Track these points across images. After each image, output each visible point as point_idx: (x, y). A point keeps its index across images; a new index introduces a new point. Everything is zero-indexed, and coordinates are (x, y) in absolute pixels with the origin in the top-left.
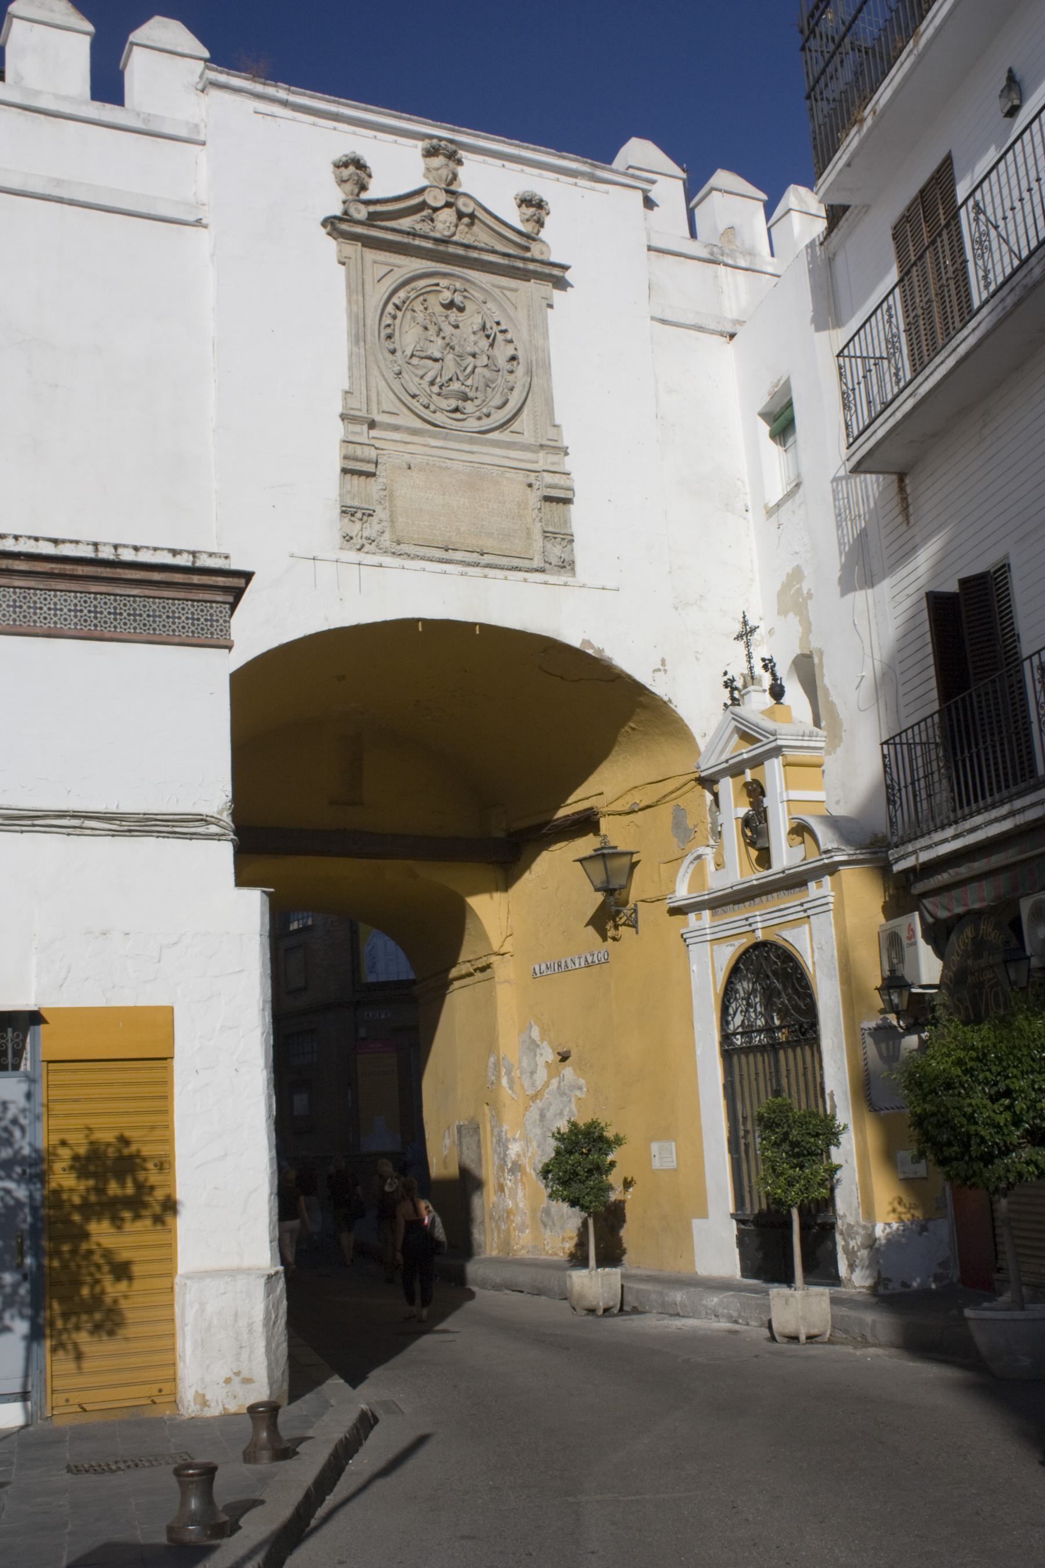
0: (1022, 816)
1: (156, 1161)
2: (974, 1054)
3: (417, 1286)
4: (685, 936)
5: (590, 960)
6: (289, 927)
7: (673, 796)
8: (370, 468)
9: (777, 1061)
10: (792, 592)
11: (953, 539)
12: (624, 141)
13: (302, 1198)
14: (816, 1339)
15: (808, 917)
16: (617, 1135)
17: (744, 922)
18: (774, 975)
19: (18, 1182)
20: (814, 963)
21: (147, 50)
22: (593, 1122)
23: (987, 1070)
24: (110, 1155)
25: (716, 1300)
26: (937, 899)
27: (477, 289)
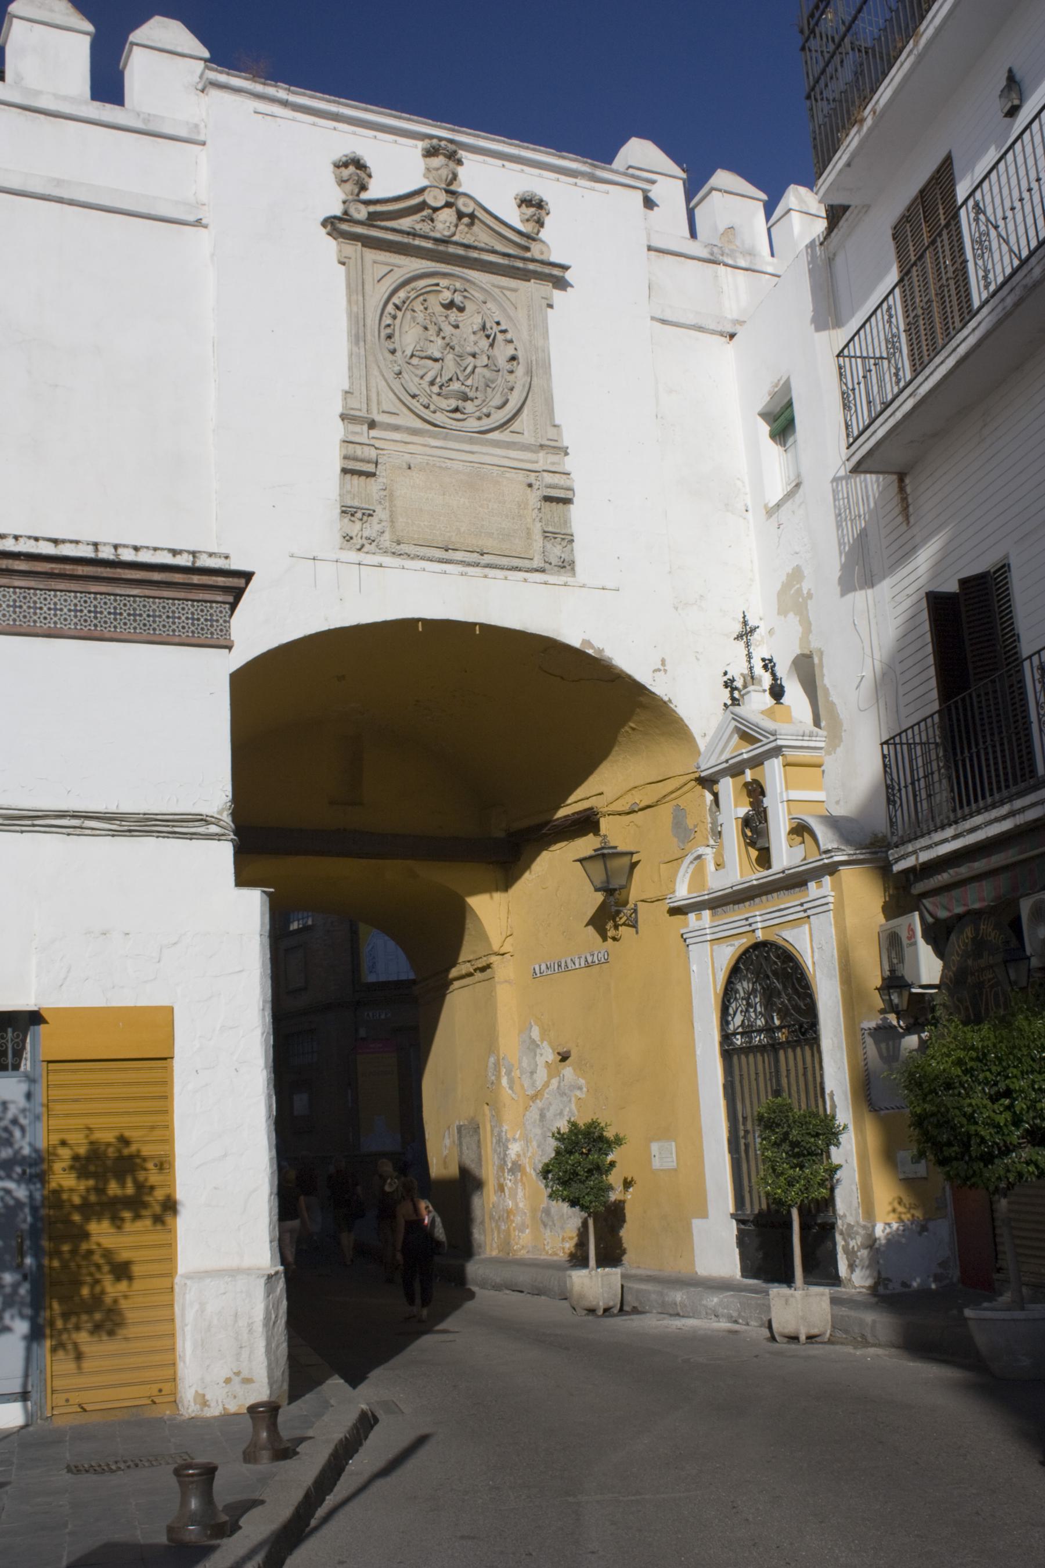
0: (1022, 816)
1: (156, 1161)
2: (974, 1054)
3: (417, 1286)
4: (685, 936)
5: (590, 960)
6: (289, 927)
7: (673, 796)
8: (370, 468)
9: (777, 1061)
10: (792, 592)
11: (953, 539)
12: (624, 141)
13: (302, 1198)
14: (816, 1339)
15: (808, 917)
16: (617, 1135)
17: (744, 922)
18: (774, 975)
19: (18, 1182)
20: (814, 963)
21: (147, 50)
22: (593, 1122)
23: (987, 1070)
24: (110, 1155)
25: (716, 1300)
26: (937, 899)
27: (477, 289)
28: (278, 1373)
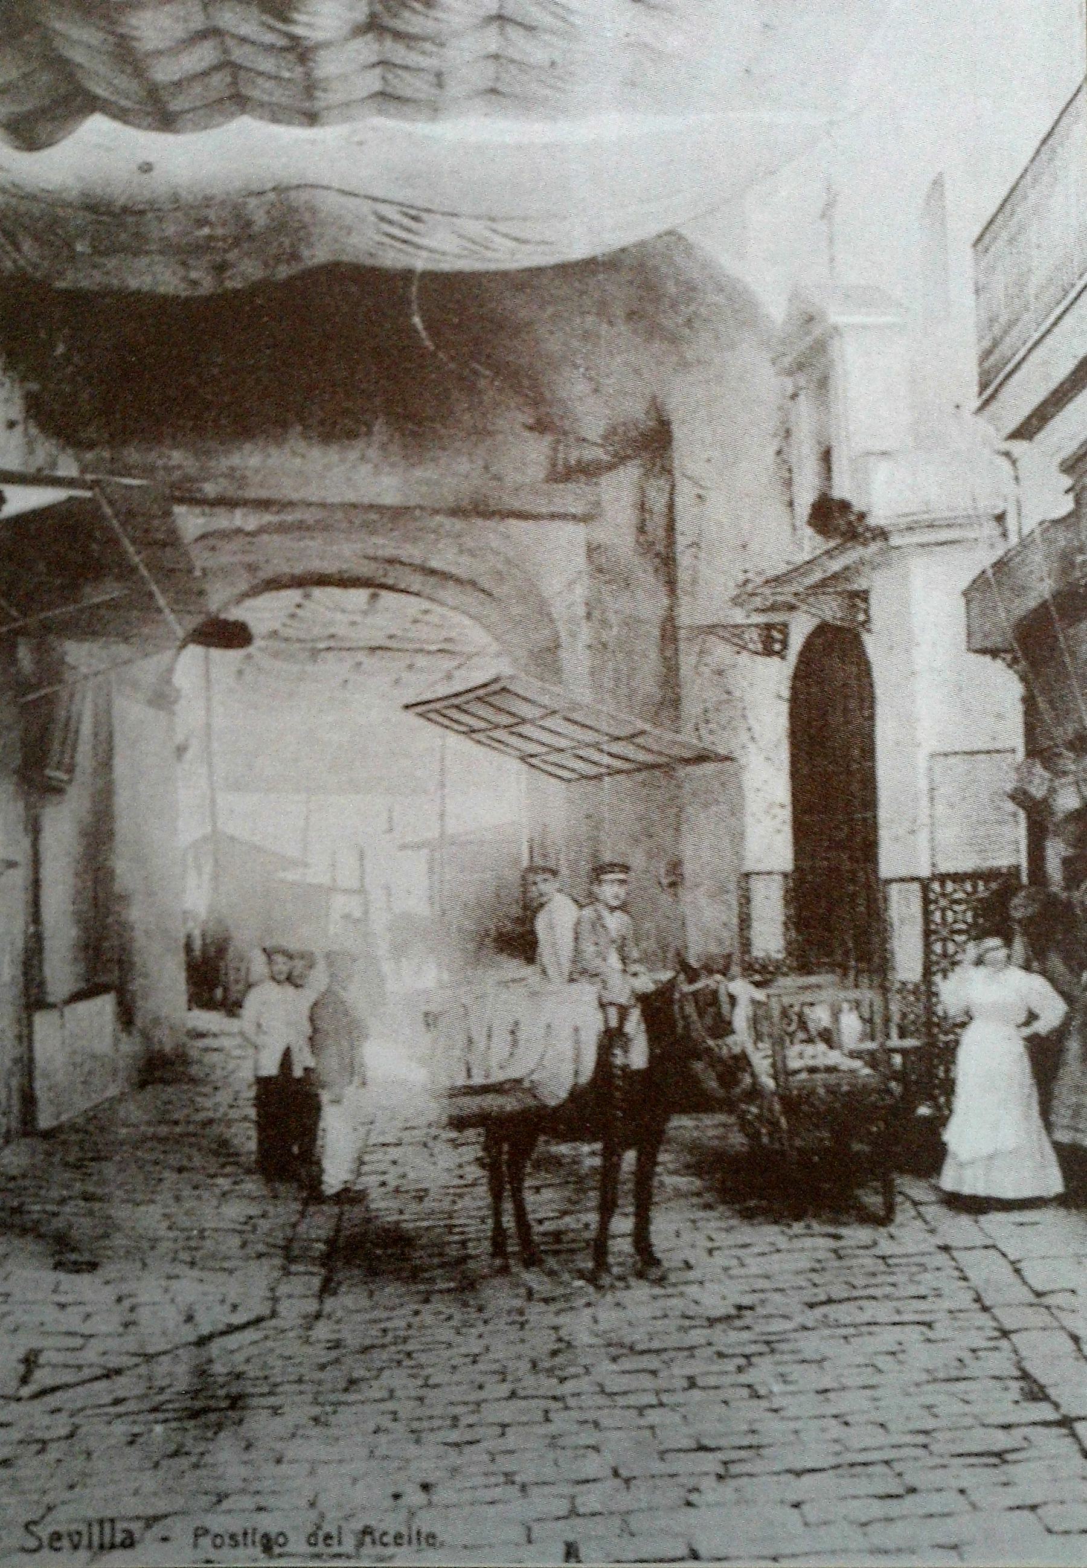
13: (48, 772)
28: (392, 111)
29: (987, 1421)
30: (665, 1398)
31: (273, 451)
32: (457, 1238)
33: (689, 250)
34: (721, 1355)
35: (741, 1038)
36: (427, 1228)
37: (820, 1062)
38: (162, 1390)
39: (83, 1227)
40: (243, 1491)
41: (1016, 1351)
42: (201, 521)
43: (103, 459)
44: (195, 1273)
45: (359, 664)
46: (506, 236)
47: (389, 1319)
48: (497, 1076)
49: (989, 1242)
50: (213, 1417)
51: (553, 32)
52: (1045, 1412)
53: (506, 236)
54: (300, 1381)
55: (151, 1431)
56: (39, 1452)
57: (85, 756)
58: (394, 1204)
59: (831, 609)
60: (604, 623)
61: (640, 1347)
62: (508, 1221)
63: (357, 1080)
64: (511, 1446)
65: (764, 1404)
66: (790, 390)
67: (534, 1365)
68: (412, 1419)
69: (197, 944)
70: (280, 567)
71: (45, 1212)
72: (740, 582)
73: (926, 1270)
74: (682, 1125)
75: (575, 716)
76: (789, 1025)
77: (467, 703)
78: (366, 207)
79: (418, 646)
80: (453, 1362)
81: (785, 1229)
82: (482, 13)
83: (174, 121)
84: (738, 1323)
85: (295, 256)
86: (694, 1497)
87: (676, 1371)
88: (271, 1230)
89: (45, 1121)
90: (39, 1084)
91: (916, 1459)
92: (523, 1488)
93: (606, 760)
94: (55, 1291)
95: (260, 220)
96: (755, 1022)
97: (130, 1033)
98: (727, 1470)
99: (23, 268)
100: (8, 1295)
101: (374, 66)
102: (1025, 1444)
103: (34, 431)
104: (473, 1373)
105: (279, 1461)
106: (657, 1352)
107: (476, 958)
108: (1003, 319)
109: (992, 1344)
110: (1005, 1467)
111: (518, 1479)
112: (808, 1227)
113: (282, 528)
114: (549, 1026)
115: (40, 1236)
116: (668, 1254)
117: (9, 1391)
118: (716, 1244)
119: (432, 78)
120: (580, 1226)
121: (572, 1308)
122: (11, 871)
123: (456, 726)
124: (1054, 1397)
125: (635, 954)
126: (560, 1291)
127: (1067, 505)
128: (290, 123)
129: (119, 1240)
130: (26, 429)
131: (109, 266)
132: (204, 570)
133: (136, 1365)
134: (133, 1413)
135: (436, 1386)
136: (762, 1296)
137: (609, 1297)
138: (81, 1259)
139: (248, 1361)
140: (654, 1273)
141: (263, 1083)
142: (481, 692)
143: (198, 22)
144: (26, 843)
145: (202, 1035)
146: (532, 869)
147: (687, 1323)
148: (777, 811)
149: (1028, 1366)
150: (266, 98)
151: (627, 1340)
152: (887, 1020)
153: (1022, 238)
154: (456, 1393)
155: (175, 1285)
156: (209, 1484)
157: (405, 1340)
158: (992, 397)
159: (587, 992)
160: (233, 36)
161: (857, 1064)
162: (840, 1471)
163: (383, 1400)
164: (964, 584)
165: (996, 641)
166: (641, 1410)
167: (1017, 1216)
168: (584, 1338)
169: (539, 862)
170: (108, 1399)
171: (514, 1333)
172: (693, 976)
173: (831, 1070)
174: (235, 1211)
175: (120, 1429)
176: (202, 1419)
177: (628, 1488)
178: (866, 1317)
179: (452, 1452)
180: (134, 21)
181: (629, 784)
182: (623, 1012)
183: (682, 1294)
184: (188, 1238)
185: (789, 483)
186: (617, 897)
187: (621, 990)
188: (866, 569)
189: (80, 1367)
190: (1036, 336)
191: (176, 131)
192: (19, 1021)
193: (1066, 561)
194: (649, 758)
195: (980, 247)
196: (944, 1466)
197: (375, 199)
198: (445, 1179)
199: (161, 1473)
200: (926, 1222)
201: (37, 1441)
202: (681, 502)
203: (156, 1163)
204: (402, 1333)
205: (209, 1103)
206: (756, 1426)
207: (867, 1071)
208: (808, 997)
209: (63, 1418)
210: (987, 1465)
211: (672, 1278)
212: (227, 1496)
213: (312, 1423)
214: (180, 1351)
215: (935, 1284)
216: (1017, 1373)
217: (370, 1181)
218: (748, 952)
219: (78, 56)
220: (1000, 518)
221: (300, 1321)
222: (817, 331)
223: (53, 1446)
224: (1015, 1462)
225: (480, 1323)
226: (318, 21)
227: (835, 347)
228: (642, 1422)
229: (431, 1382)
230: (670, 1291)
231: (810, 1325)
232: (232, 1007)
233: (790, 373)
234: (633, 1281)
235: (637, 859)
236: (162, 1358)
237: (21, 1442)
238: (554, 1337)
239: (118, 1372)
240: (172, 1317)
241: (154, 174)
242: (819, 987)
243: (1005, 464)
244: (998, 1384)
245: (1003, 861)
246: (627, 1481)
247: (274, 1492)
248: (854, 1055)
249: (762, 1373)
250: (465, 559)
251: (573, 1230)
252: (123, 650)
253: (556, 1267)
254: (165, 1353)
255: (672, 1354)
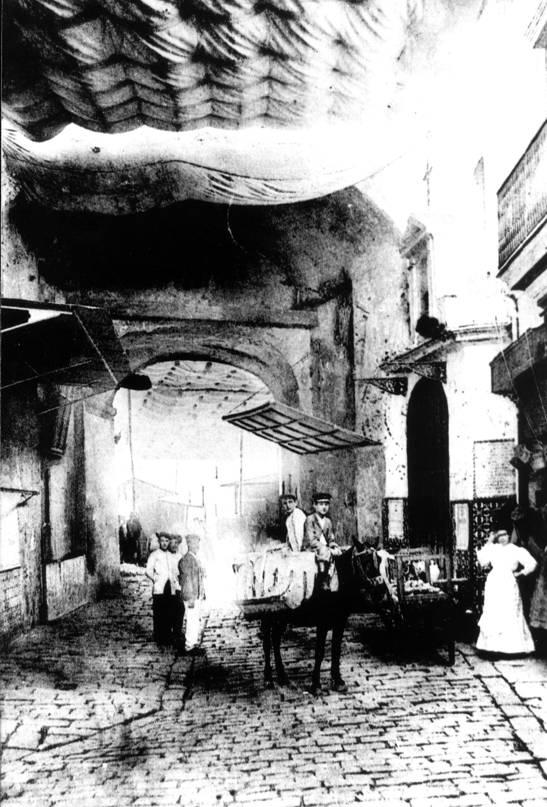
29: (498, 760)
30: (346, 748)
31: (161, 293)
32: (248, 671)
33: (360, 195)
34: (372, 727)
35: (383, 576)
36: (234, 667)
37: (420, 588)
38: (107, 746)
39: (69, 667)
40: (145, 796)
41: (512, 727)
42: (126, 327)
43: (77, 296)
44: (124, 689)
45: (202, 397)
46: (271, 188)
47: (216, 710)
48: (267, 595)
49: (499, 674)
50: (132, 759)
51: (295, 85)
52: (526, 756)
53: (271, 188)
54: (173, 741)
55: (102, 766)
56: (48, 777)
57: (70, 440)
58: (219, 656)
59: (427, 371)
60: (319, 378)
61: (334, 723)
62: (272, 664)
63: (201, 597)
64: (273, 772)
65: (393, 751)
66: (408, 265)
67: (284, 731)
68: (226, 759)
69: (125, 531)
70: (163, 349)
71: (51, 661)
72: (384, 358)
73: (469, 687)
74: (356, 618)
75: (304, 422)
76: (406, 571)
77: (253, 416)
78: (204, 172)
79: (230, 389)
80: (246, 731)
81: (403, 667)
82: (261, 75)
83: (110, 127)
84: (380, 712)
85: (171, 197)
86: (360, 797)
87: (351, 734)
88: (160, 668)
89: (51, 617)
90: (49, 599)
91: (465, 778)
92: (279, 792)
93: (321, 444)
94: (55, 699)
95: (153, 178)
96: (389, 570)
97: (92, 574)
98: (375, 783)
99: (36, 201)
100: (33, 701)
101: (208, 101)
102: (517, 772)
103: (43, 282)
104: (256, 736)
105: (163, 780)
106: (342, 725)
107: (258, 539)
108: (511, 231)
109: (500, 723)
110: (508, 783)
111: (276, 788)
112: (413, 666)
113: (164, 331)
114: (292, 571)
115: (48, 673)
116: (347, 679)
117: (34, 747)
118: (370, 674)
119: (235, 107)
120: (307, 666)
121: (302, 705)
122: (35, 497)
123: (248, 427)
124: (530, 748)
125: (333, 537)
126: (296, 696)
127: (541, 321)
128: (167, 129)
129: (87, 674)
130: (39, 282)
131: (79, 200)
132: (127, 351)
133: (95, 734)
134: (92, 758)
135: (239, 742)
136: (390, 699)
137: (320, 700)
138: (68, 683)
139: (148, 731)
140: (341, 688)
141: (156, 597)
142: (260, 411)
143: (122, 77)
144: (42, 483)
145: (128, 575)
146: (284, 496)
147: (356, 712)
148: (401, 468)
149: (518, 733)
150: (155, 116)
151: (329, 720)
152: (452, 568)
153: (522, 191)
154: (248, 746)
155: (114, 695)
156: (128, 792)
157: (224, 721)
158: (506, 268)
159: (310, 556)
160: (138, 84)
161: (437, 589)
162: (429, 784)
163: (213, 750)
164: (491, 359)
165: (505, 386)
166: (335, 754)
167: (513, 662)
168: (308, 719)
169: (287, 492)
170: (81, 751)
171: (274, 717)
172: (360, 547)
173: (426, 592)
174: (143, 659)
175: (87, 765)
176: (126, 761)
177: (329, 792)
178: (441, 710)
179: (245, 775)
180: (90, 77)
181: (330, 456)
182: (327, 565)
183: (354, 698)
184: (120, 673)
185: (407, 311)
186: (324, 510)
187: (326, 554)
188: (444, 352)
189: (67, 736)
190: (527, 238)
191: (112, 132)
192: (39, 569)
193: (540, 347)
194: (341, 443)
195: (502, 193)
196: (477, 782)
197: (209, 169)
198: (242, 643)
199: (106, 786)
200: (469, 664)
201: (46, 771)
202: (356, 320)
203: (106, 636)
204: (222, 717)
205: (130, 607)
206: (389, 761)
207: (441, 593)
208: (415, 558)
209: (59, 760)
210: (498, 781)
211: (349, 690)
212: (138, 798)
213: (178, 761)
214: (116, 727)
215: (475, 694)
216: (512, 737)
217: (208, 644)
218: (387, 536)
219: (62, 93)
220: (509, 328)
221: (174, 712)
222: (421, 236)
223: (54, 773)
224: (513, 780)
225: (259, 712)
226: (180, 78)
227: (431, 245)
228: (335, 759)
229: (236, 740)
230: (348, 696)
231: (415, 712)
232: (142, 562)
233: (408, 257)
234: (331, 692)
235: (334, 493)
236: (107, 731)
237: (39, 771)
238: (294, 719)
239: (86, 738)
240: (112, 710)
241: (100, 153)
242: (420, 553)
243: (511, 301)
244: (503, 742)
245: (508, 492)
246: (328, 788)
247: (159, 796)
248: (435, 585)
249: (392, 736)
250: (252, 346)
251: (303, 668)
252: (89, 390)
253: (295, 685)
254: (108, 728)
255: (350, 727)
